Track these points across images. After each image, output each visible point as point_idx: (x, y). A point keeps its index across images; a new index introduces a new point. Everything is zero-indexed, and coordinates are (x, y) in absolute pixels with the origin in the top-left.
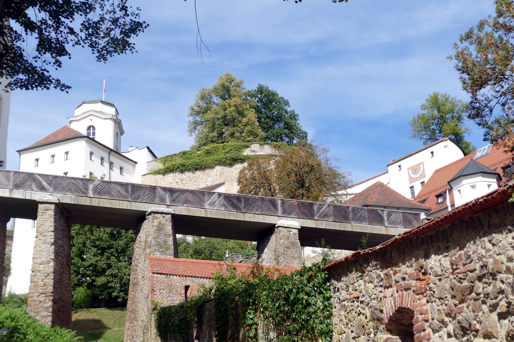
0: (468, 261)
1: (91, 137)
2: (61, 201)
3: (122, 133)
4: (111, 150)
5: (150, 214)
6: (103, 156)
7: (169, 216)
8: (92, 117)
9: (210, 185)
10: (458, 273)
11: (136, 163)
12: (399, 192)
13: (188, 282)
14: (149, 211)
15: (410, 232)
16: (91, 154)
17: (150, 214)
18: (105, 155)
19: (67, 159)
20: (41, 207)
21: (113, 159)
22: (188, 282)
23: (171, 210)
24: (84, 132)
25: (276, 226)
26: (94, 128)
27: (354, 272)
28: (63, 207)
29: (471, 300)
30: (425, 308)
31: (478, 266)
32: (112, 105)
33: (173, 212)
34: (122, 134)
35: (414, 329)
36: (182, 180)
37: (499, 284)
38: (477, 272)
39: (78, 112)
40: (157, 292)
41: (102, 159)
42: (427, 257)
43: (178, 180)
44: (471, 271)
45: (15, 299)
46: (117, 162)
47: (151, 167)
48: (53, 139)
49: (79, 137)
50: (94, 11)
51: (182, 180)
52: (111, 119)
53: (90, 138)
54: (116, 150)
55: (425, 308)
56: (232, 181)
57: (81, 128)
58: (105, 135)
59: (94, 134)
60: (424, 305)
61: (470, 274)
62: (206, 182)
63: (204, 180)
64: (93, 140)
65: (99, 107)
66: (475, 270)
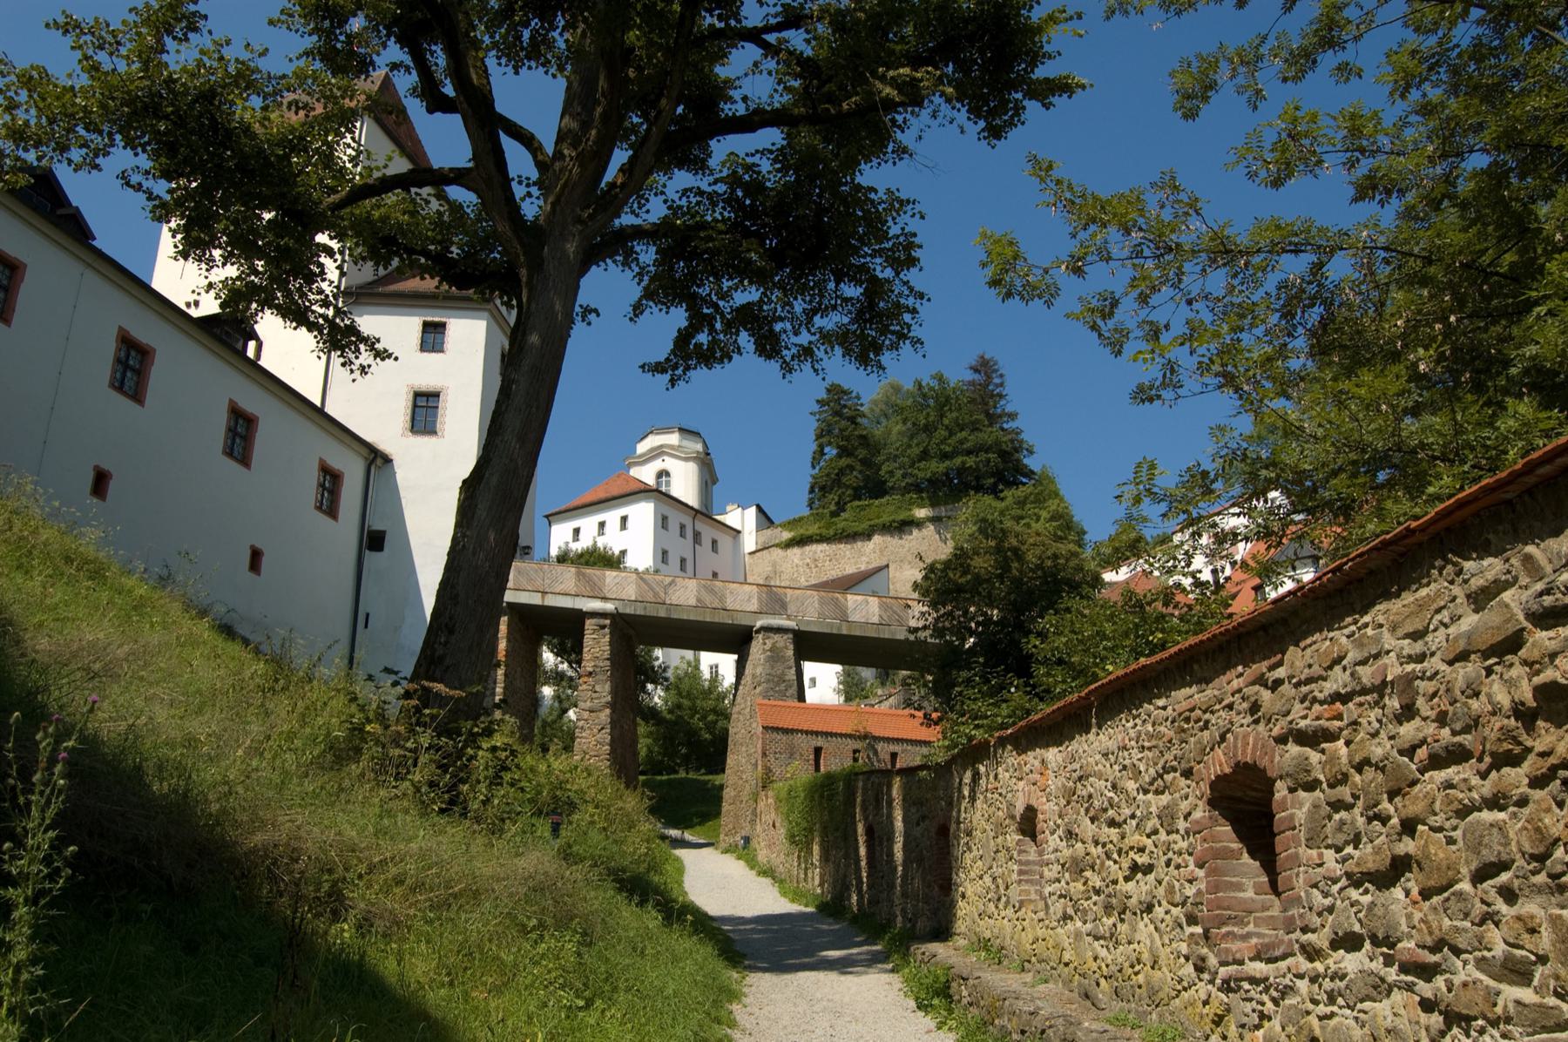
1: (663, 489)
3: (714, 481)
4: (697, 511)
5: (758, 632)
9: (863, 568)
13: (820, 742)
14: (759, 624)
16: (665, 518)
17: (758, 632)
18: (688, 521)
20: (590, 624)
21: (700, 526)
22: (820, 742)
26: (668, 474)
27: (1094, 730)
32: (697, 434)
34: (714, 483)
39: (642, 448)
40: (771, 757)
41: (682, 527)
45: (123, 354)
46: (708, 533)
50: (673, 382)
58: (685, 484)
65: (673, 439)
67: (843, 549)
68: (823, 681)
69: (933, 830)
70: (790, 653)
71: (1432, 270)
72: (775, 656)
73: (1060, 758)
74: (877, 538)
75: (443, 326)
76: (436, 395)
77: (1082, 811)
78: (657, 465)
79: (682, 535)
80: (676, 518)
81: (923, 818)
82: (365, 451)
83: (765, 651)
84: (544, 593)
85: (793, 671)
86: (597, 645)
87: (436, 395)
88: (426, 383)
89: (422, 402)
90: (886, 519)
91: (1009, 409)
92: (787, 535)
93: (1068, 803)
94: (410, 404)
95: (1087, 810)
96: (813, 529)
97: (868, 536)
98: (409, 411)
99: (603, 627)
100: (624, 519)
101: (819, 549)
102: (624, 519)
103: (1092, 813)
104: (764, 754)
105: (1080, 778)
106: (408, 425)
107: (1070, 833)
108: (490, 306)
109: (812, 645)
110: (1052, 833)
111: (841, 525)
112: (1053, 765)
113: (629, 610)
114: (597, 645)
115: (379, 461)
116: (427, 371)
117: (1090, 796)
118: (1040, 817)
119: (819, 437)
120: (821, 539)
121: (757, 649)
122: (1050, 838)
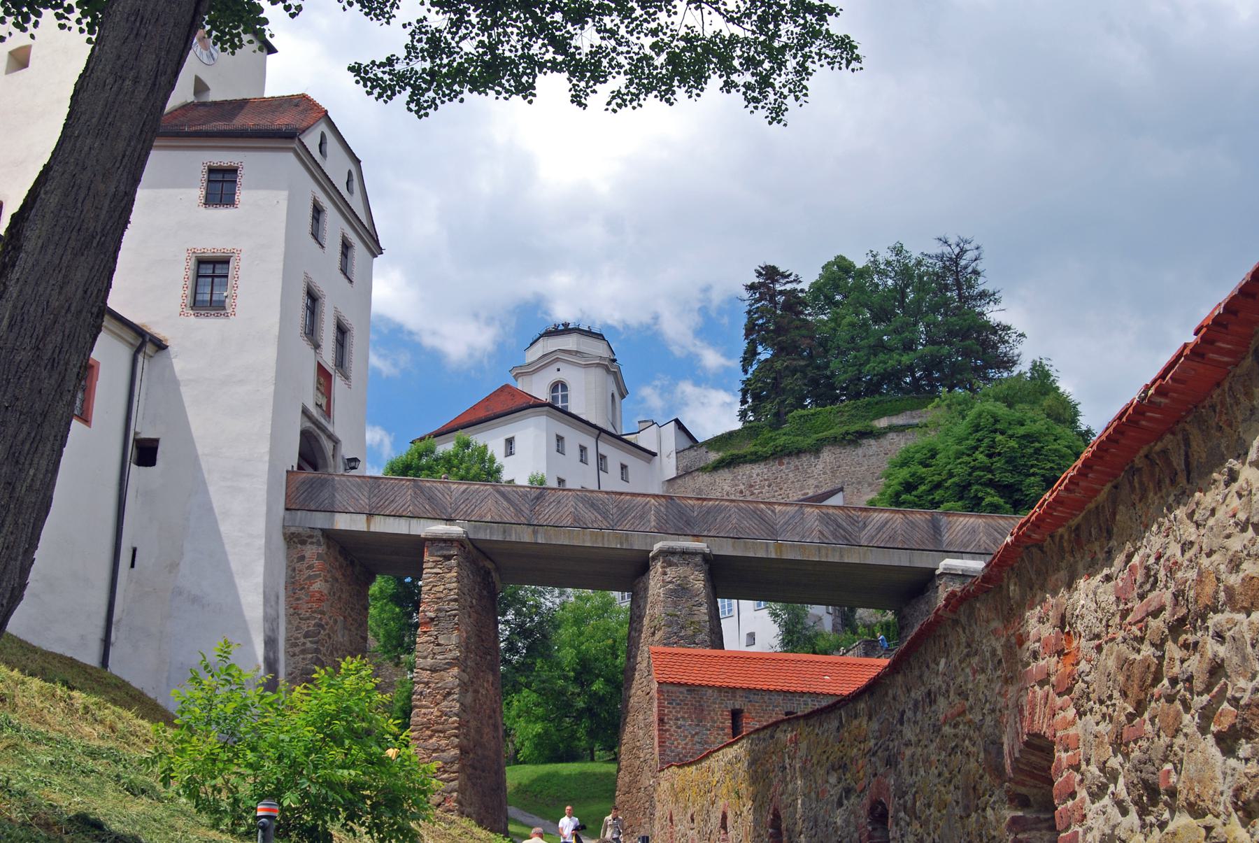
0: (1148, 586)
1: (560, 405)
2: (471, 536)
4: (601, 430)
6: (584, 444)
7: (698, 559)
8: (558, 365)
10: (1130, 624)
11: (654, 454)
12: (286, 94)
14: (657, 547)
15: (1028, 521)
16: (560, 439)
18: (589, 442)
19: (511, 454)
21: (605, 449)
23: (701, 546)
24: (543, 394)
25: (938, 572)
26: (564, 387)
28: (475, 547)
29: (1157, 700)
30: (1072, 731)
31: (1167, 597)
33: (707, 550)
34: (623, 396)
35: (1055, 792)
36: (751, 486)
37: (1212, 648)
38: (1166, 615)
41: (583, 449)
42: (1070, 585)
43: (742, 487)
44: (1155, 614)
47: (685, 462)
48: (482, 414)
49: (535, 405)
51: (751, 486)
52: (598, 365)
53: (557, 409)
54: (611, 430)
55: (1072, 731)
56: (859, 483)
57: (539, 388)
59: (565, 398)
60: (1073, 723)
61: (1153, 623)
62: (802, 488)
63: (797, 485)
64: (564, 411)
66: (1161, 609)
67: (786, 470)
68: (751, 625)
69: (863, 812)
70: (700, 585)
71: (1166, 682)
72: (680, 591)
73: (1107, 595)
74: (827, 455)
75: (234, 171)
76: (225, 261)
77: (1189, 721)
78: (551, 375)
79: (583, 460)
80: (575, 438)
81: (848, 791)
82: (129, 335)
83: (665, 583)
84: (370, 515)
85: (704, 609)
86: (440, 583)
87: (225, 261)
88: (212, 245)
89: (207, 270)
90: (838, 430)
91: (989, 288)
92: (714, 456)
93: (1140, 707)
94: (191, 274)
95: (1207, 715)
96: (748, 448)
97: (816, 450)
98: (190, 283)
99: (448, 558)
100: (510, 442)
101: (755, 471)
102: (510, 442)
103: (1227, 715)
104: (661, 721)
105: (1177, 628)
106: (189, 301)
107: (1152, 791)
108: (295, 145)
109: (730, 577)
110: (1095, 797)
111: (781, 441)
112: (1088, 621)
113: (483, 535)
114: (440, 583)
115: (149, 348)
116: (216, 230)
117: (1216, 669)
118: (1062, 756)
119: (747, 336)
120: (756, 458)
121: (657, 583)
122: (1092, 809)
